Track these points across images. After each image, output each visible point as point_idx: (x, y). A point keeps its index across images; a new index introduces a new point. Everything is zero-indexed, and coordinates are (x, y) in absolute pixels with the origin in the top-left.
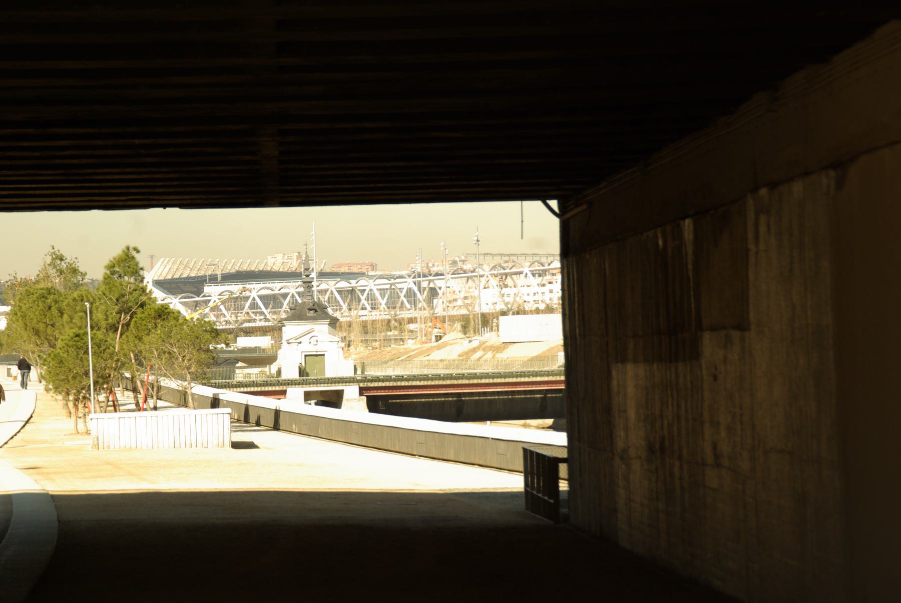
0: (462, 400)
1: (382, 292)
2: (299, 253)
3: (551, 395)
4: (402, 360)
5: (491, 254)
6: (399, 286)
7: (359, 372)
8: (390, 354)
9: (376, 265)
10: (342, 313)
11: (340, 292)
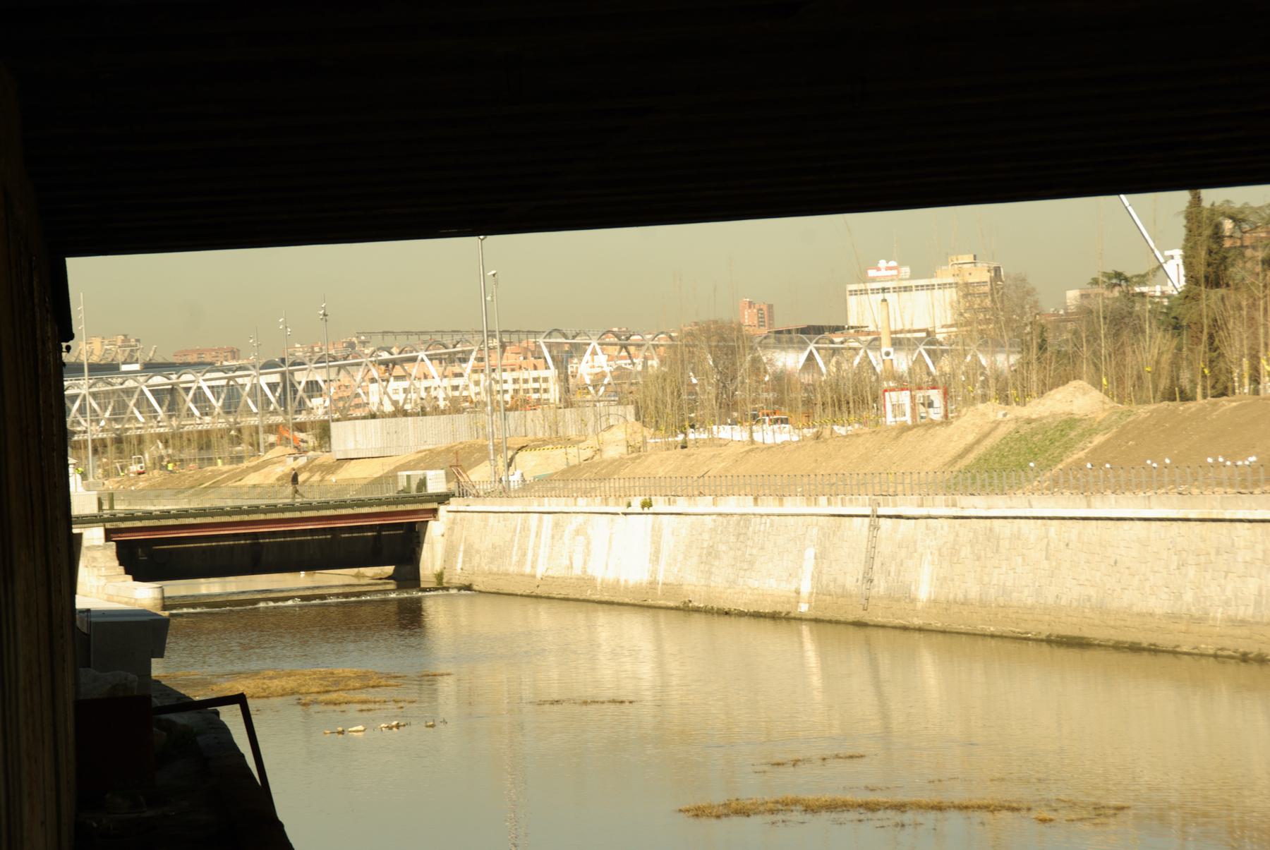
0: (260, 543)
1: (273, 387)
2: (125, 336)
3: (387, 533)
4: (205, 487)
5: (393, 332)
6: (240, 381)
7: (106, 507)
8: (191, 479)
9: (238, 350)
10: (159, 422)
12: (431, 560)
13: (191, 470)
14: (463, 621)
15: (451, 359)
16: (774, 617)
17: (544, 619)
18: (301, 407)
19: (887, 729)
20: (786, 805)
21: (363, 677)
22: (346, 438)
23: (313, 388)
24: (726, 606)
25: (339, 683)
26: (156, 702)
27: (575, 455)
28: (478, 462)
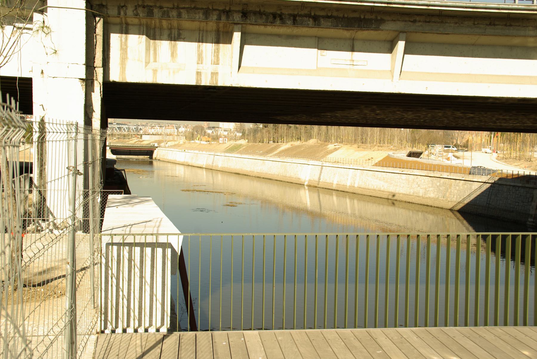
1: (135, 128)
11: (117, 127)
12: (154, 156)
13: (122, 140)
14: (158, 165)
15: (161, 127)
16: (200, 167)
17: (169, 165)
18: (139, 132)
19: (214, 183)
20: (194, 190)
21: (143, 170)
22: (144, 137)
23: (141, 129)
24: (194, 165)
25: (139, 171)
26: (115, 170)
27: (176, 143)
28: (162, 143)
